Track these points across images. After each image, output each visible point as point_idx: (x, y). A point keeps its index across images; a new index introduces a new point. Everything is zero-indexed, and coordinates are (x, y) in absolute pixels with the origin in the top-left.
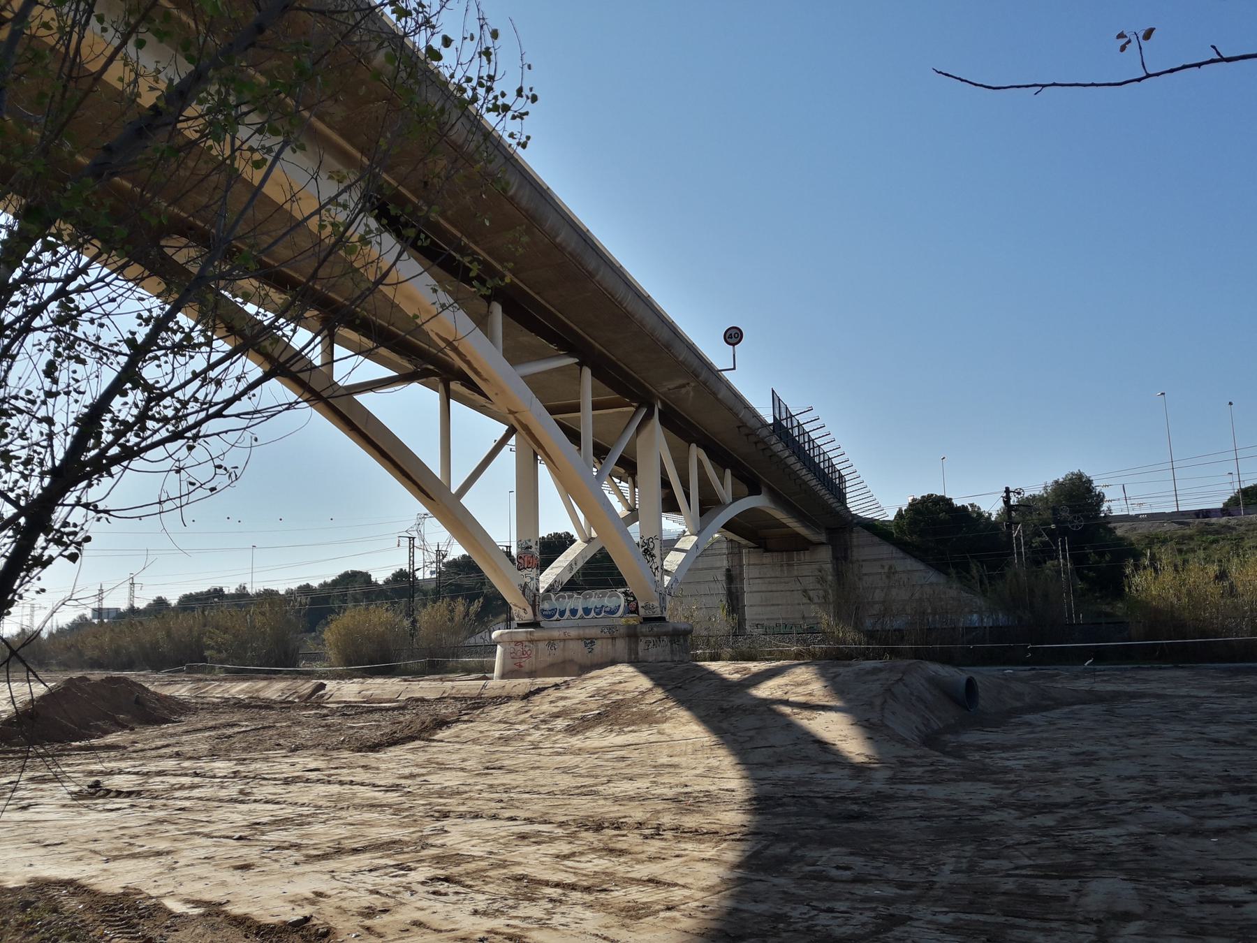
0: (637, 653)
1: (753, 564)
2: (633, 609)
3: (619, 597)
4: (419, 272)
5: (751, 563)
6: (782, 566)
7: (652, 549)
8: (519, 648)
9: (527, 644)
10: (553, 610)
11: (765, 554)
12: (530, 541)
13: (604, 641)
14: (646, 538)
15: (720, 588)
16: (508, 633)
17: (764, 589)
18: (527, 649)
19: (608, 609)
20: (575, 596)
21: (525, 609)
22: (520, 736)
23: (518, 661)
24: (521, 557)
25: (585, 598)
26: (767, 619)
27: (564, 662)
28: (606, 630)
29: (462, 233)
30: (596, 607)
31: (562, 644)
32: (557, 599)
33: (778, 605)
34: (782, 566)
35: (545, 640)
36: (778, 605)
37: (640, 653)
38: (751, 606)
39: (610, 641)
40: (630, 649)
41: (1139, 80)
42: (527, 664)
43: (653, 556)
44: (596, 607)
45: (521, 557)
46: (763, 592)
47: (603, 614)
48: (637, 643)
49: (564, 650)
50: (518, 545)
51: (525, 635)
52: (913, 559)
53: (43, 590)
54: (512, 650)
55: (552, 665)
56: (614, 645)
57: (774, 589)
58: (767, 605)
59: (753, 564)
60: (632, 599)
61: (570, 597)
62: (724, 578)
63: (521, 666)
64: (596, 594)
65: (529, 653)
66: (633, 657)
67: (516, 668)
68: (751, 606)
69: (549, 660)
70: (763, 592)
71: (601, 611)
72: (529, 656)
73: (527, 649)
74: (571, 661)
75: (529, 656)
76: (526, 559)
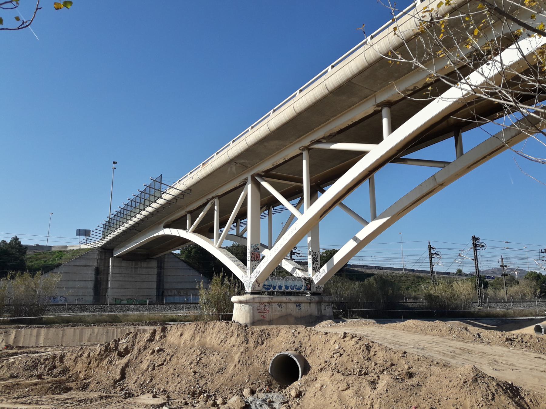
0: (321, 312)
1: (116, 266)
2: (309, 288)
3: (302, 281)
4: (514, 48)
5: (115, 265)
6: (132, 268)
7: (317, 258)
8: (262, 306)
9: (266, 304)
10: (270, 285)
11: (123, 261)
12: (258, 245)
13: (306, 304)
14: (314, 252)
15: (91, 276)
16: (258, 297)
17: (121, 279)
18: (267, 307)
19: (297, 287)
20: (281, 279)
21: (259, 284)
22: (102, 359)
23: (262, 314)
24: (253, 254)
25: (286, 280)
26: (122, 296)
27: (287, 315)
28: (309, 299)
29: (401, 11)
30: (291, 286)
31: (285, 305)
32: (272, 280)
33: (128, 288)
34: (132, 268)
35: (276, 303)
36: (128, 288)
37: (323, 312)
38: (113, 288)
39: (308, 304)
40: (318, 309)
41: (12, 8)
42: (268, 316)
43: (317, 261)
44: (291, 286)
45: (253, 254)
46: (120, 281)
47: (295, 289)
48: (321, 306)
49: (286, 309)
50: (251, 246)
51: (268, 299)
52: (194, 270)
53: (80, 233)
54: (258, 308)
55: (281, 317)
56: (310, 307)
57: (127, 280)
58: (122, 288)
59: (116, 266)
60: (308, 283)
61: (279, 279)
62: (94, 272)
63: (264, 317)
64: (291, 278)
65: (268, 309)
66: (320, 313)
67: (262, 318)
68: (113, 288)
69: (279, 314)
70: (120, 281)
71: (294, 288)
72: (268, 312)
73: (267, 307)
74: (291, 315)
75: (268, 312)
76: (256, 255)
